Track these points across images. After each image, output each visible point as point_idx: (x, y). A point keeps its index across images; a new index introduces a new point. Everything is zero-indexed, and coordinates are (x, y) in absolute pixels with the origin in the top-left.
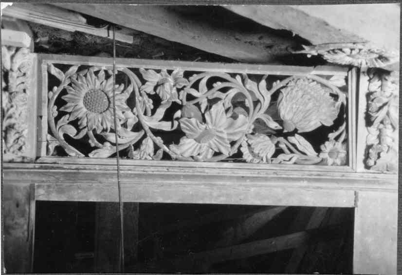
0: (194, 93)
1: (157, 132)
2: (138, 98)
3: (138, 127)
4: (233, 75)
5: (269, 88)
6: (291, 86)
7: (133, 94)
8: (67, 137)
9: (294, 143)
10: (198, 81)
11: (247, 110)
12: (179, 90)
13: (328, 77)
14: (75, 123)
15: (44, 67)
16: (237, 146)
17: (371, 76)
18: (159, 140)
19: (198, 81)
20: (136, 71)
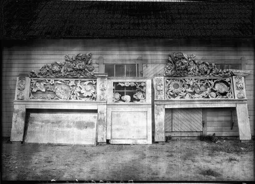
0: (197, 83)
1: (189, 92)
2: (185, 85)
3: (185, 92)
4: (205, 79)
5: (213, 81)
6: (29, 176)
7: (184, 84)
8: (170, 95)
9: (206, 169)
10: (198, 81)
11: (209, 86)
12: (194, 83)
13: (225, 79)
14: (172, 91)
15: (165, 80)
16: (207, 95)
17: (72, 83)
18: (190, 94)
19: (198, 81)
20: (184, 79)
